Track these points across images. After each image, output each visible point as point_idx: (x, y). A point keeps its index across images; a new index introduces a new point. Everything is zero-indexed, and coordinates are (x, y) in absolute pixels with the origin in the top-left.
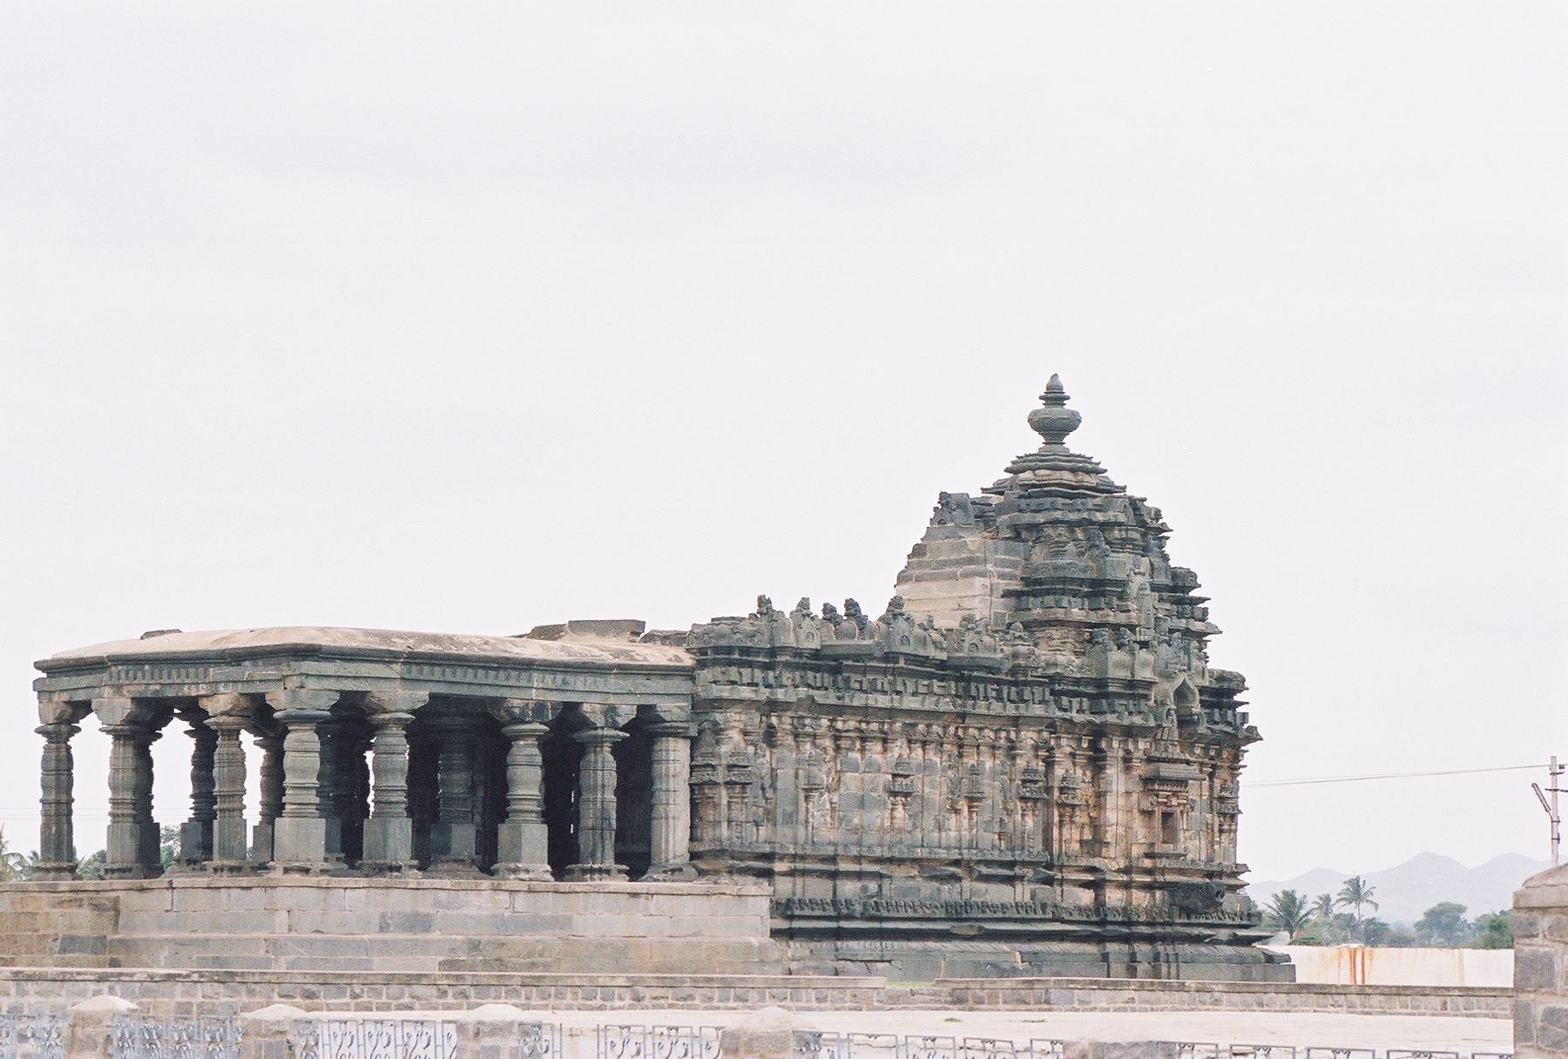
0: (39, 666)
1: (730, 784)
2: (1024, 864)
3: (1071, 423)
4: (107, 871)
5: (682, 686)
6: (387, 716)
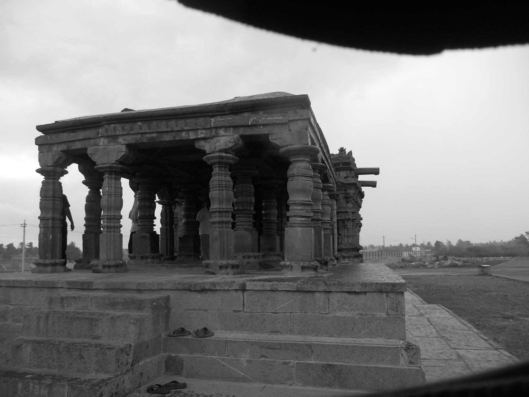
0: (40, 128)
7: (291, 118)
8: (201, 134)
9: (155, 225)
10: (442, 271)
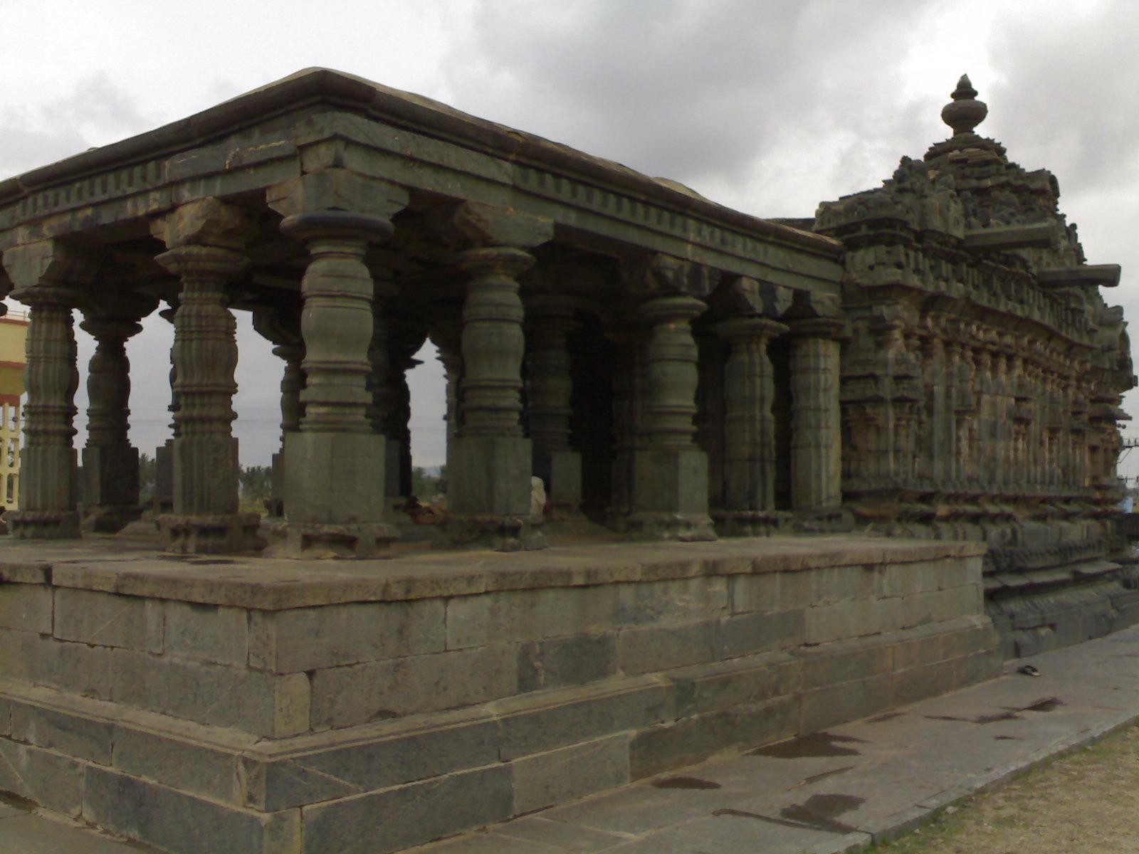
1: (899, 401)
2: (1077, 499)
3: (979, 113)
5: (830, 270)
6: (494, 251)
7: (302, 141)
8: (155, 202)
9: (170, 426)
10: (437, 563)
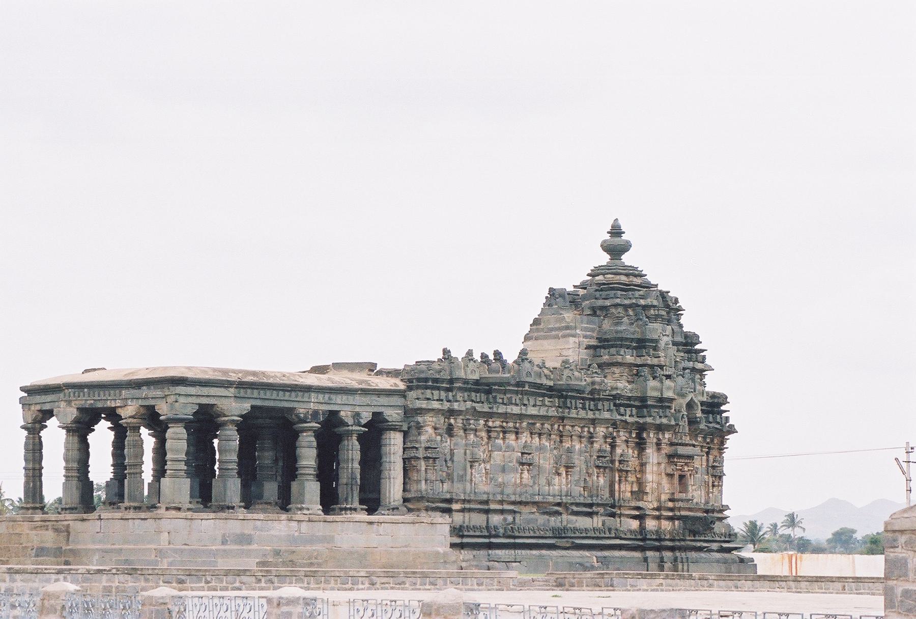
0: (23, 389)
1: (426, 458)
2: (598, 505)
3: (626, 247)
4: (62, 509)
5: (399, 401)
6: (226, 419)
